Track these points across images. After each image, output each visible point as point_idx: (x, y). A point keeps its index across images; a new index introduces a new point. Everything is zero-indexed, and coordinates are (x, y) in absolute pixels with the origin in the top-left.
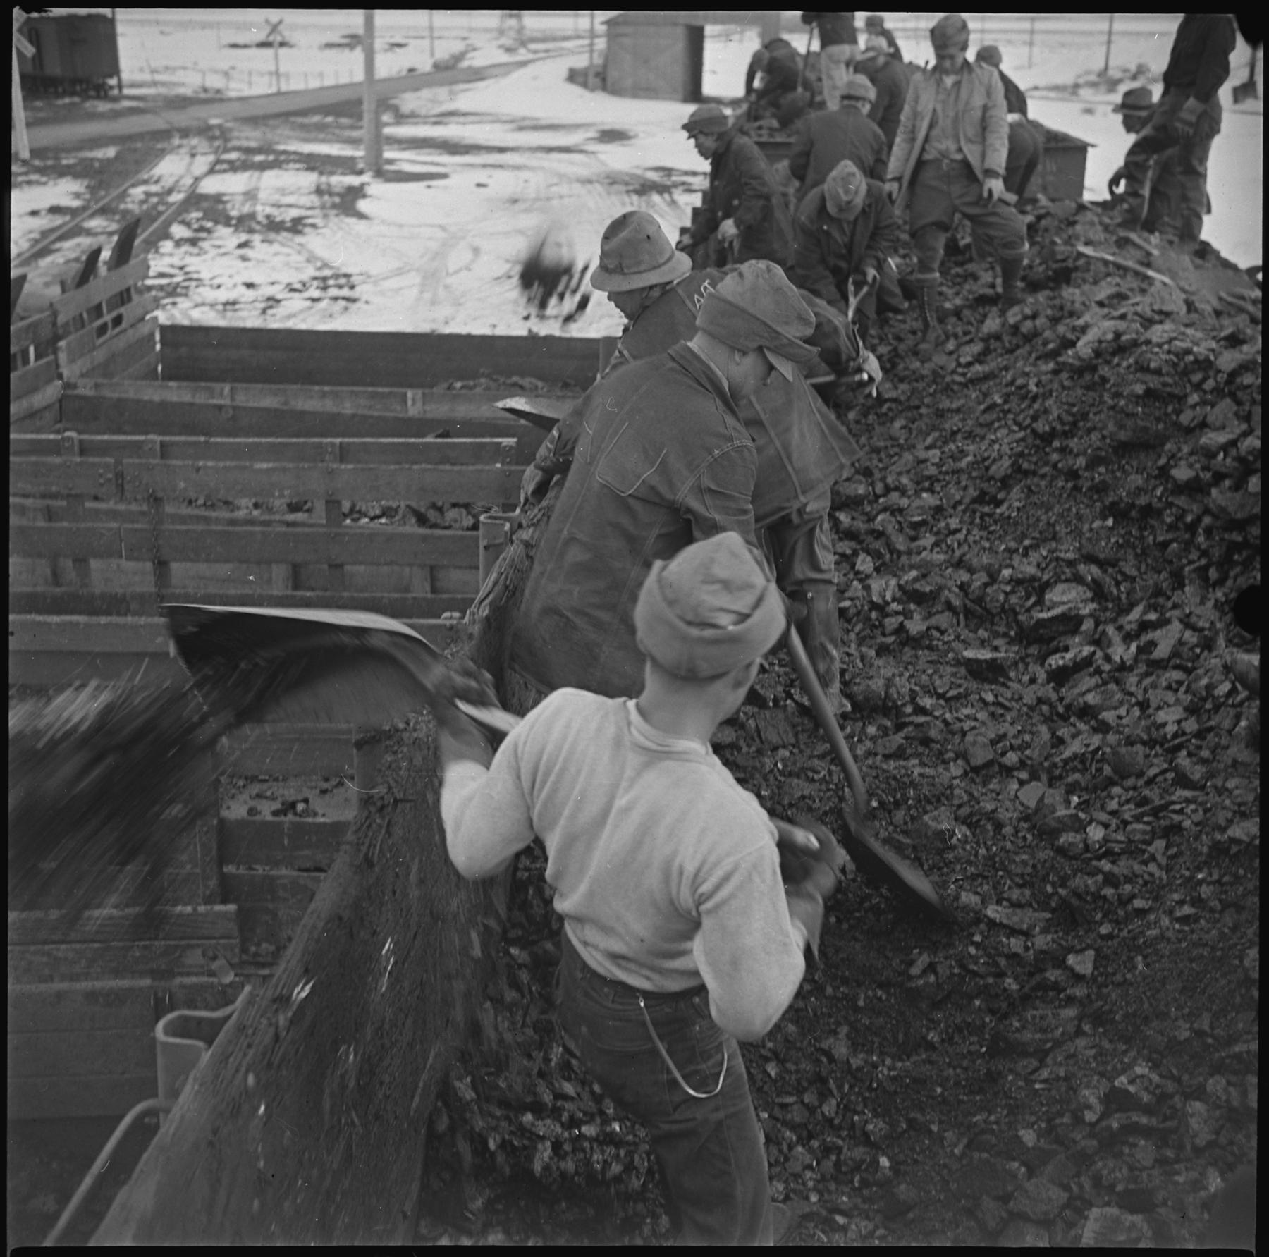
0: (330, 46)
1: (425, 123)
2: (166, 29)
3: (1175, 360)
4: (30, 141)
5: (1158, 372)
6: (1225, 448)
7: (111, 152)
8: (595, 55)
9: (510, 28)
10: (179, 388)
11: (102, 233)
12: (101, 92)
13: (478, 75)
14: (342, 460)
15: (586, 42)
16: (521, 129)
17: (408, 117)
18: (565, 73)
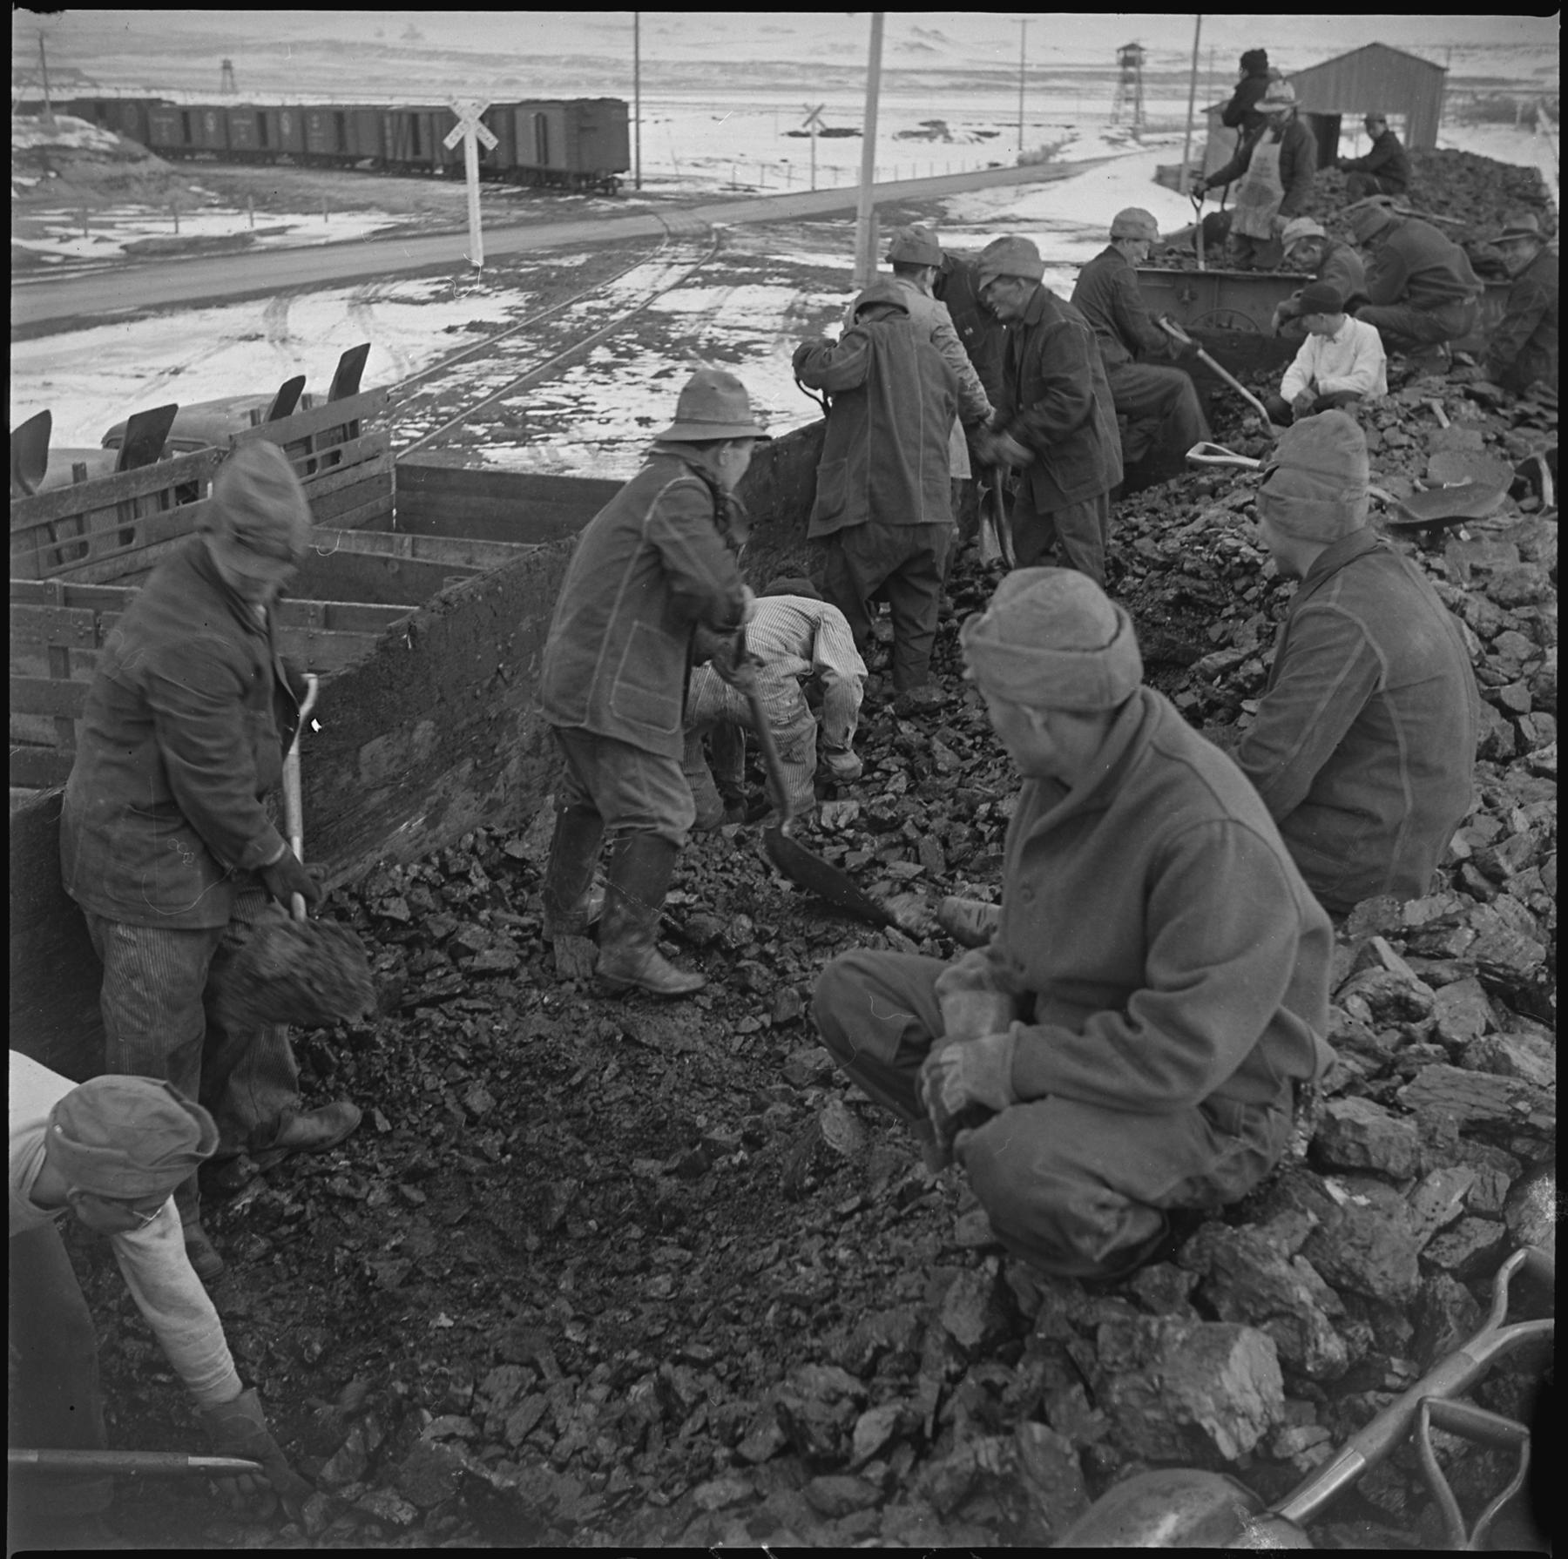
0: (906, 135)
1: (965, 231)
2: (717, 114)
3: (1220, 561)
4: (485, 248)
5: (1195, 574)
6: (1226, 671)
7: (580, 260)
8: (1192, 150)
9: (1127, 114)
10: (358, 536)
11: (511, 355)
12: (609, 189)
13: (1063, 173)
14: (327, 626)
15: (1183, 135)
16: (1080, 240)
17: (953, 223)
18: (1153, 172)
